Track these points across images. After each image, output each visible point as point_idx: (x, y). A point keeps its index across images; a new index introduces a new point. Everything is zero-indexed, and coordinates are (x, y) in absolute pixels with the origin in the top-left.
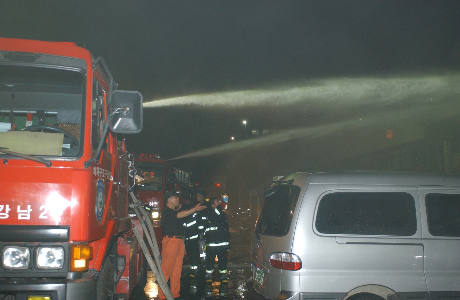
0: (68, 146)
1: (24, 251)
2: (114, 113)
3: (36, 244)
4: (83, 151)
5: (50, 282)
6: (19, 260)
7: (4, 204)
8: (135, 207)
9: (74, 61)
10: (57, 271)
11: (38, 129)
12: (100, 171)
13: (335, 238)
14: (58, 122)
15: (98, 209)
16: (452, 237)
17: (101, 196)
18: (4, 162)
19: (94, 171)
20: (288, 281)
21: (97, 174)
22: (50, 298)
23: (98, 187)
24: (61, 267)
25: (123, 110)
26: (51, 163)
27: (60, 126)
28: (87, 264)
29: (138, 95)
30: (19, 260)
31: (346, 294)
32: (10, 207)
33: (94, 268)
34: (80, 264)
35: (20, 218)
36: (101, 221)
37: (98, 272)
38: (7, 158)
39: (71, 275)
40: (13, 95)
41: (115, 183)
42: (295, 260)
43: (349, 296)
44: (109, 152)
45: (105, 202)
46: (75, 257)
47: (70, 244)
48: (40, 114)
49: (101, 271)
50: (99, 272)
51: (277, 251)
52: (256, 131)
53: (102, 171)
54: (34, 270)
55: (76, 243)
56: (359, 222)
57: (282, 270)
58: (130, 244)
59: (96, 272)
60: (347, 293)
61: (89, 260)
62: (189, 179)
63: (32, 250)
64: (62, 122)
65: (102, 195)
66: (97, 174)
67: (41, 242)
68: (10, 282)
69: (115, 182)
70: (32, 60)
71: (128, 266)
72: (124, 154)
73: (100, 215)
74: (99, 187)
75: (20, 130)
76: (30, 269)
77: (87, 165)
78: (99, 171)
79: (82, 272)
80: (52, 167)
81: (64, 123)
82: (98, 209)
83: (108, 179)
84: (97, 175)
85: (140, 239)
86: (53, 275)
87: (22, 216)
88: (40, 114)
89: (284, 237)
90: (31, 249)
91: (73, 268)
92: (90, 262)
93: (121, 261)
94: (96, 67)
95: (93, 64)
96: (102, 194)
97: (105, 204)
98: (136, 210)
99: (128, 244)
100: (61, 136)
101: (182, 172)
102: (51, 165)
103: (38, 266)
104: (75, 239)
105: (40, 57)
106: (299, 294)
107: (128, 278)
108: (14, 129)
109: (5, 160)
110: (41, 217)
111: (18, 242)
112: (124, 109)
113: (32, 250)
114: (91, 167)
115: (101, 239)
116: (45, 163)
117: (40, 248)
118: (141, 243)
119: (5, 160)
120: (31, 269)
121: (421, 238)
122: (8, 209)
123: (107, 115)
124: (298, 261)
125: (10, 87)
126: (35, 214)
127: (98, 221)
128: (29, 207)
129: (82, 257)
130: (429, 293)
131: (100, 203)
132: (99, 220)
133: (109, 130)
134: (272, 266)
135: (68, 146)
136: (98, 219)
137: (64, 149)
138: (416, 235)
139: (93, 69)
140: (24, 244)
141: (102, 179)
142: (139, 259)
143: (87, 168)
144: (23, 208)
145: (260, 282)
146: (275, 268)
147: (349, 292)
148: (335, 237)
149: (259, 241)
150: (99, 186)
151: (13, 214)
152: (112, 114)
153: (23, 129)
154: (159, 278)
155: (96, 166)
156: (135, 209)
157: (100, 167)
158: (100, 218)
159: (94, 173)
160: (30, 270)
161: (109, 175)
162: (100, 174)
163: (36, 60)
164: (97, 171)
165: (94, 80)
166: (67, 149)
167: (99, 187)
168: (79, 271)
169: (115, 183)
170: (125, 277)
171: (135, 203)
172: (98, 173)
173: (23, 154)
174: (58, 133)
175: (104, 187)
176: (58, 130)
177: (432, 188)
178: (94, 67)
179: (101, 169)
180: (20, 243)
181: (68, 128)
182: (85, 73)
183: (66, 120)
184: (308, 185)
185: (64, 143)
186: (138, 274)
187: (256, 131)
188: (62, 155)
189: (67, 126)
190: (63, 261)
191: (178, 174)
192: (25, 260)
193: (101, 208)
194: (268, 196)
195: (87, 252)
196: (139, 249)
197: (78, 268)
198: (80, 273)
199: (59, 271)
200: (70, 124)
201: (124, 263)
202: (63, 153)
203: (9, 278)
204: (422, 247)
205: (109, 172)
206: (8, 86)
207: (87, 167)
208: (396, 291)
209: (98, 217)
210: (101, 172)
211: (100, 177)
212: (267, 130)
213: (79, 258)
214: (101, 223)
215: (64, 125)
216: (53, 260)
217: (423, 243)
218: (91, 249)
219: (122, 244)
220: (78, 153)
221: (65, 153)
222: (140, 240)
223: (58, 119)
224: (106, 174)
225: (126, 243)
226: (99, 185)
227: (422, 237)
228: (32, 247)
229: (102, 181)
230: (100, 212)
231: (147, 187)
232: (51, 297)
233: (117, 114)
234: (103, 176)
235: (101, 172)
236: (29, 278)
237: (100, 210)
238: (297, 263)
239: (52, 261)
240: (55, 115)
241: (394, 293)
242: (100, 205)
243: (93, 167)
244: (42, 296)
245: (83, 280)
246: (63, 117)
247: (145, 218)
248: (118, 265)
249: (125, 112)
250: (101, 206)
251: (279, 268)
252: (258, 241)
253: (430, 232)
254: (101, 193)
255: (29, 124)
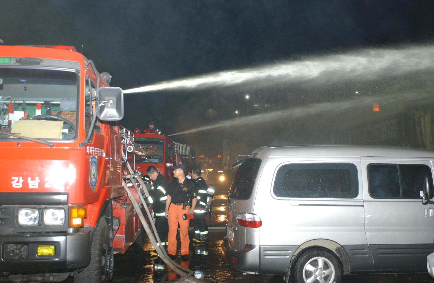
0: (66, 131)
1: (34, 212)
2: (100, 105)
3: (43, 206)
4: (78, 135)
5: (54, 235)
6: (31, 219)
7: (18, 176)
8: (131, 177)
9: (70, 64)
10: (60, 227)
11: (45, 118)
12: (93, 149)
13: (289, 201)
14: (61, 110)
15: (91, 180)
16: (389, 199)
17: (94, 169)
18: (18, 144)
19: (87, 150)
20: (250, 237)
21: (90, 152)
22: (54, 247)
23: (91, 162)
24: (63, 224)
25: (108, 102)
26: (54, 145)
27: (63, 114)
28: (83, 221)
29: (119, 90)
30: (31, 219)
31: (299, 247)
32: (23, 179)
33: (90, 226)
34: (77, 221)
35: (30, 187)
36: (95, 189)
37: (93, 229)
38: (19, 141)
39: (71, 230)
40: (25, 88)
41: (107, 159)
42: (257, 220)
43: (301, 248)
44: (102, 133)
45: (98, 174)
46: (73, 216)
47: (69, 207)
48: (47, 104)
49: (96, 228)
50: (94, 229)
51: (242, 212)
52: (258, 105)
53: (95, 150)
54: (42, 226)
55: (73, 206)
56: (320, 187)
57: (246, 227)
58: (125, 208)
59: (91, 229)
60: (300, 246)
61: (84, 218)
62: (190, 152)
63: (41, 211)
64: (64, 110)
65: (95, 168)
66: (90, 152)
67: (47, 205)
68: (25, 235)
69: (107, 157)
70: (38, 63)
71: (124, 226)
72: (118, 134)
73: (94, 184)
74: (92, 163)
75: (30, 119)
76: (39, 226)
77: (81, 145)
78: (91, 150)
79: (79, 228)
80: (54, 148)
81: (66, 111)
82: (92, 179)
83: (100, 156)
84: (90, 153)
85: (135, 205)
86: (57, 230)
87: (32, 186)
88: (47, 104)
89: (248, 200)
90: (40, 210)
91: (72, 225)
92: (85, 220)
93: (116, 221)
94: (87, 67)
95: (85, 66)
96: (95, 167)
97: (98, 175)
98: (132, 180)
99: (124, 208)
100: (61, 123)
101: (183, 145)
102: (53, 146)
103: (45, 223)
104: (72, 202)
105: (43, 61)
106: (260, 247)
107: (124, 236)
108: (27, 117)
109: (18, 143)
110: (47, 186)
111: (30, 205)
112: (108, 101)
113: (41, 211)
114: (84, 147)
115: (95, 202)
116: (48, 145)
117: (46, 210)
118: (136, 208)
119: (18, 143)
120: (40, 225)
121: (362, 200)
122: (21, 180)
123: (95, 107)
124: (259, 220)
125: (23, 82)
126: (41, 184)
127: (92, 189)
128: (37, 178)
129: (78, 216)
130: (369, 246)
131: (94, 175)
132: (93, 188)
133: (97, 118)
134: (239, 224)
135: (66, 131)
136: (92, 187)
137: (63, 134)
138: (359, 198)
139: (86, 69)
140: (34, 207)
141: (94, 156)
142: (135, 221)
143: (81, 148)
144: (33, 179)
145: (231, 238)
146: (242, 226)
147: (301, 245)
148: (290, 200)
149: (230, 204)
150: (92, 161)
151: (25, 184)
152: (99, 106)
153: (31, 119)
154: (151, 236)
155: (90, 146)
156: (131, 179)
157: (93, 147)
158: (93, 187)
159: (87, 152)
160: (39, 227)
161: (101, 153)
162: (92, 152)
163: (41, 64)
164: (90, 150)
165: (87, 78)
166: (66, 133)
167: (92, 163)
168: (77, 227)
169: (107, 159)
170: (121, 235)
171: (131, 174)
172: (91, 152)
173: (32, 138)
174: (59, 121)
175: (97, 162)
176: (59, 118)
177: (373, 159)
178: (86, 68)
179: (93, 148)
180: (31, 206)
181: (70, 115)
182: (79, 73)
183: (68, 109)
184: (268, 158)
185: (64, 128)
186: (135, 234)
187: (258, 105)
188: (62, 138)
189: (68, 113)
190: (64, 220)
191: (179, 148)
192: (35, 219)
193: (94, 178)
194: (236, 167)
195: (82, 212)
196: (135, 213)
197: (76, 225)
198: (78, 229)
199: (61, 227)
200: (71, 111)
201: (118, 223)
202: (62, 136)
203: (24, 233)
204: (362, 207)
205: (101, 150)
206: (20, 81)
207: (81, 147)
208: (341, 244)
209: (92, 185)
210: (94, 151)
211: (92, 155)
212: (268, 104)
213: (76, 216)
214: (95, 190)
215: (66, 113)
216: (57, 219)
217: (364, 204)
218: (86, 210)
219: (118, 208)
220: (74, 136)
221: (64, 136)
222: (135, 205)
223: (61, 107)
224: (98, 152)
225: (121, 207)
226: (92, 160)
227: (363, 200)
228: (40, 209)
229: (95, 158)
230: (94, 182)
231: (150, 160)
232: (55, 247)
233: (103, 106)
234: (96, 153)
235: (94, 151)
236: (39, 232)
237: (94, 180)
238: (259, 222)
239: (56, 219)
240: (58, 105)
241: (339, 246)
242: (94, 176)
243: (86, 147)
244: (49, 245)
245: (80, 233)
246: (65, 106)
247: (141, 186)
248: (113, 224)
249: (110, 104)
250: (94, 177)
251: (243, 226)
252: (229, 205)
253: (370, 196)
254: (94, 167)
255: (38, 112)
